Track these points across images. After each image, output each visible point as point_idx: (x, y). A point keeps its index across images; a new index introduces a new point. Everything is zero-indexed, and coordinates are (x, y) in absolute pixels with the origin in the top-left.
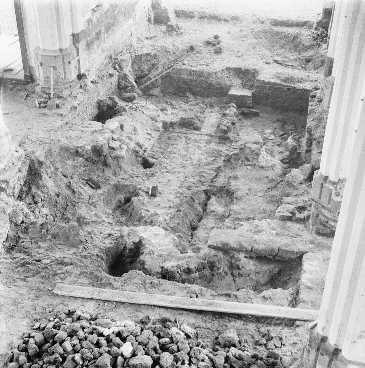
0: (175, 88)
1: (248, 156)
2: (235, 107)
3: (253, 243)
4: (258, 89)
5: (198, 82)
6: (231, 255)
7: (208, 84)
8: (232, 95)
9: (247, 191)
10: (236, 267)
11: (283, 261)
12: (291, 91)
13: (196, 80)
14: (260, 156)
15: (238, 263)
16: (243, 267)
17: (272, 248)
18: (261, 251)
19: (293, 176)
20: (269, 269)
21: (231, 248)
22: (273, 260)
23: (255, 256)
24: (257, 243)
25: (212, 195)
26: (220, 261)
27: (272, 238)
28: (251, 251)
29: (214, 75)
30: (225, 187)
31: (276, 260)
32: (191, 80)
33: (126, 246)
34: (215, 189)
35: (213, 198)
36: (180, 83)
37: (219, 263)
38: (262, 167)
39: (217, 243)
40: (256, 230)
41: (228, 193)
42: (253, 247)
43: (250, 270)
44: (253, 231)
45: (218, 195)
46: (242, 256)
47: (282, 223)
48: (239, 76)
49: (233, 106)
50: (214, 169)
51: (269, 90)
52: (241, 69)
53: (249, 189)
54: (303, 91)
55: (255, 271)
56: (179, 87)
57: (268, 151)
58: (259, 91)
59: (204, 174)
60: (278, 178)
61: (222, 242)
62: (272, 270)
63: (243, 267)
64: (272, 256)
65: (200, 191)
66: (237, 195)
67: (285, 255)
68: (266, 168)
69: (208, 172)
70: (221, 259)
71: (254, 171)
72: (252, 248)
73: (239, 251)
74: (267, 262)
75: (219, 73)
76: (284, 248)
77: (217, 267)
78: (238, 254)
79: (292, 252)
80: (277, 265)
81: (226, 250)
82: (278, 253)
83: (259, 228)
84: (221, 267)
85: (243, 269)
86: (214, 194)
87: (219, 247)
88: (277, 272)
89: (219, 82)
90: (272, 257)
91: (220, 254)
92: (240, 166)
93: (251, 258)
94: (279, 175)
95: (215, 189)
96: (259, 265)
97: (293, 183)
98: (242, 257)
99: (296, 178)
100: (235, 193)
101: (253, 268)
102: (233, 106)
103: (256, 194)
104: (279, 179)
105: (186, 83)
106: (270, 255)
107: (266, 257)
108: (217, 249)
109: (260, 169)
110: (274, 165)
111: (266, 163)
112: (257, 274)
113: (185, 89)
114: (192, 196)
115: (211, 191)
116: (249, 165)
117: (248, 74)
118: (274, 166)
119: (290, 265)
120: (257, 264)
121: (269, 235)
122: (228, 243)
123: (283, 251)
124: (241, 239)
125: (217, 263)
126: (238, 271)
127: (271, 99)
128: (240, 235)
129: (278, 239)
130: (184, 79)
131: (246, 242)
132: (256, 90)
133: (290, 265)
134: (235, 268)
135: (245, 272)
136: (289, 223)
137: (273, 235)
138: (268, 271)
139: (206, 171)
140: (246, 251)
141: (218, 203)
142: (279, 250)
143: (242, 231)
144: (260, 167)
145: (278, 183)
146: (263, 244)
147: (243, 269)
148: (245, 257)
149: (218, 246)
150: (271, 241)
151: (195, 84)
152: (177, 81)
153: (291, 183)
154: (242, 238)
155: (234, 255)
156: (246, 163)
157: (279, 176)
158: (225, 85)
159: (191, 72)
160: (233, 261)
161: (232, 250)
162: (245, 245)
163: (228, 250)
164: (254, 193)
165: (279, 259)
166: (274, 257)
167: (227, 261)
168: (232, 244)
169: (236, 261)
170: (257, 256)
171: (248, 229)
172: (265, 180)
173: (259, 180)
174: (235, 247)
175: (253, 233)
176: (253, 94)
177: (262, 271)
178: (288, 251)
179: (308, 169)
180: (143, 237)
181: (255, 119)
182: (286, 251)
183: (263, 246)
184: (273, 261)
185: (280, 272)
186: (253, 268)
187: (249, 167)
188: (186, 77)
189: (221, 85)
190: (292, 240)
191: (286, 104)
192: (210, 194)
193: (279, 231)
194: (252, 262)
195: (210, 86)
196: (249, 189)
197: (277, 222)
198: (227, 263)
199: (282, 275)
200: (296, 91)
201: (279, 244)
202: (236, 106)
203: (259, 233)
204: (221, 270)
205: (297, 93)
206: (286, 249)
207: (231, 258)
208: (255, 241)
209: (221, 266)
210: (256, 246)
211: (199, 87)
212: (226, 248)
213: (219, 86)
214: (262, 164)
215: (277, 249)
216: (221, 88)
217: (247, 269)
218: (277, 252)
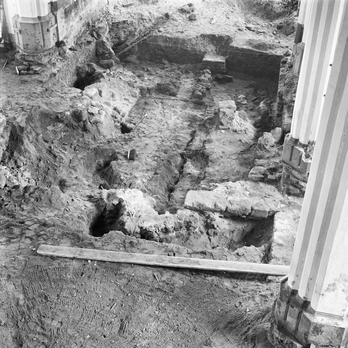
0: (151, 55)
4: (231, 56)
6: (207, 215)
11: (255, 220)
14: (234, 120)
16: (218, 226)
18: (235, 211)
19: (265, 139)
23: (229, 216)
25: (188, 158)
27: (245, 198)
31: (249, 219)
33: (106, 207)
34: (191, 152)
37: (195, 222)
38: (235, 131)
43: (225, 229)
46: (216, 216)
52: (215, 35)
53: (223, 152)
57: (241, 116)
63: (218, 226)
68: (240, 132)
69: (184, 136)
72: (226, 209)
73: (214, 211)
75: (193, 40)
80: (250, 224)
82: (251, 212)
84: (197, 227)
90: (245, 217)
91: (196, 214)
93: (226, 217)
95: (191, 152)
105: (161, 50)
109: (234, 133)
110: (247, 128)
115: (187, 155)
118: (247, 130)
120: (231, 223)
129: (251, 200)
130: (160, 46)
140: (221, 212)
144: (234, 131)
149: (194, 206)
158: (200, 51)
159: (166, 39)
160: (209, 221)
164: (228, 156)
167: (203, 220)
174: (211, 207)
180: (122, 199)
181: (228, 84)
185: (252, 231)
186: (227, 227)
194: (226, 222)
195: (185, 52)
196: (223, 152)
198: (202, 222)
200: (267, 57)
205: (269, 59)
206: (258, 208)
209: (197, 225)
211: (174, 54)
212: (202, 208)
213: (194, 53)
214: (235, 128)
216: (196, 54)
218: (250, 211)
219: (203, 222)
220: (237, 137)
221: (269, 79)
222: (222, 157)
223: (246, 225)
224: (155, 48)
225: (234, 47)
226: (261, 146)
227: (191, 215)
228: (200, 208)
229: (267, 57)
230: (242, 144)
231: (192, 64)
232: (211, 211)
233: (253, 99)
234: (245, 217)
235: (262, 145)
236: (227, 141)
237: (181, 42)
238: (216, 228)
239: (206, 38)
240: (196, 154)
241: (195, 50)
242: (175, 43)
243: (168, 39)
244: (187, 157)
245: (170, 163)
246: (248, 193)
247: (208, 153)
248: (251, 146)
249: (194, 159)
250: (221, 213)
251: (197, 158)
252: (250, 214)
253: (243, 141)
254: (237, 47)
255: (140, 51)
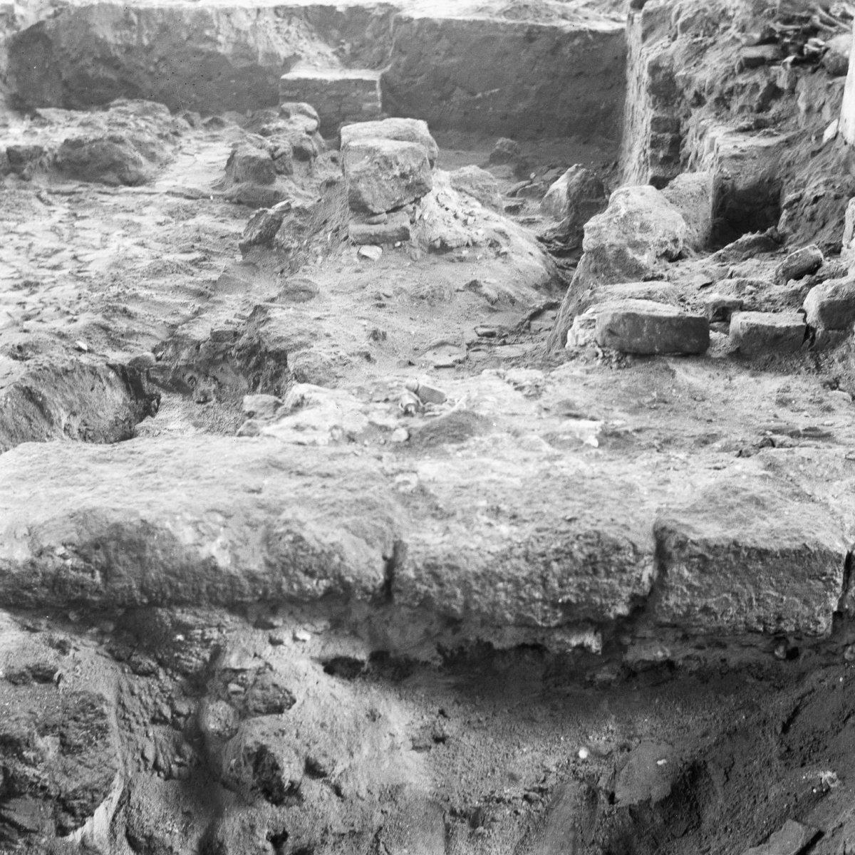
0: (66, 84)
1: (362, 186)
2: (309, 116)
3: (399, 513)
4: (404, 59)
5: (159, 52)
6: (195, 659)
7: (199, 59)
8: (298, 80)
9: (364, 344)
10: (247, 775)
11: (703, 676)
12: (540, 45)
13: (149, 49)
14: (429, 200)
15: (258, 731)
16: (312, 769)
17: (597, 539)
18: (488, 577)
19: (624, 220)
20: (573, 768)
21: (181, 573)
22: (604, 675)
23: (426, 654)
24: (439, 513)
25: (168, 389)
26: (79, 725)
27: (572, 464)
28: (389, 589)
29: (223, 19)
30: (236, 335)
31: (630, 673)
32: (129, 49)
34: (184, 354)
35: (172, 406)
36: (88, 61)
37: (66, 747)
38: (441, 249)
39: (32, 534)
40: (418, 423)
41: (259, 365)
42: (398, 547)
43: (393, 793)
44: (402, 435)
45: (204, 386)
46: (293, 655)
47: (632, 377)
48: (326, 38)
49: (303, 112)
50: (193, 287)
51: (450, 53)
52: (332, 8)
53: (375, 335)
54: (587, 42)
55: (439, 804)
56: (82, 77)
57: (467, 188)
58: (409, 68)
59: (132, 308)
60: (534, 294)
61: (81, 518)
62: (604, 770)
63: (312, 769)
64: (597, 623)
65: (93, 371)
66: (301, 361)
67: (729, 606)
68: (465, 252)
69: (159, 299)
70: (90, 705)
71: (400, 267)
72: (391, 565)
73: (263, 604)
74: (544, 698)
75: (243, 16)
76: (711, 531)
77: (41, 792)
78: (260, 636)
79: (802, 562)
80: (645, 723)
81: (131, 607)
82: (659, 585)
83: (443, 412)
84: (96, 794)
85: (314, 790)
86: (179, 387)
87: (56, 582)
88: (659, 791)
89: (247, 47)
90: (592, 641)
91: (88, 667)
92: (327, 252)
93: (390, 669)
94: (536, 278)
95: (184, 354)
96: (470, 741)
97: (630, 252)
98: (304, 664)
99: (644, 228)
100: (290, 356)
101: (416, 773)
102: (303, 112)
103: (415, 360)
104: (539, 300)
105: (110, 62)
106: (577, 617)
107: (538, 649)
108: (39, 608)
109: (433, 258)
110: (502, 233)
111: (457, 225)
112: (463, 828)
113: (109, 84)
114: (30, 383)
115: (163, 370)
116: (374, 241)
117: (364, 23)
118: (502, 240)
119: (781, 703)
120: (450, 728)
121: (547, 448)
122: (147, 528)
123: (710, 560)
124: (280, 487)
125: (48, 744)
126: (267, 812)
127: (459, 95)
128: (273, 465)
129: (635, 470)
130: (102, 44)
131: (333, 511)
132: (398, 65)
133: (781, 703)
134: (234, 785)
135: (333, 812)
136: (689, 375)
137: (578, 444)
138: (574, 790)
139: (143, 293)
140: (336, 603)
141: (196, 425)
142: (662, 556)
143: (300, 437)
145: (537, 314)
146: (497, 512)
147: (314, 790)
148: (332, 666)
149: (51, 564)
150: (571, 485)
151: (148, 63)
152: (74, 55)
153: (620, 253)
154: (297, 482)
155: (217, 652)
156: (356, 228)
157: (536, 287)
158: (272, 56)
159: (127, 15)
160: (216, 716)
161: (194, 603)
162: (321, 532)
163: (159, 598)
164: (404, 356)
165: (659, 653)
166: (617, 633)
167: (157, 720)
168: (187, 536)
169: (244, 713)
170: (449, 640)
171: (358, 426)
172: (465, 299)
173: (428, 300)
174: (224, 561)
175: (398, 447)
176: (384, 79)
177: (508, 791)
178: (763, 554)
179: (703, 192)
182: (740, 560)
183: (504, 529)
184: (606, 685)
185: (686, 791)
186: (416, 773)
187: (373, 252)
188: (108, 34)
189: (255, 57)
190: (771, 466)
191: (521, 106)
192: (156, 389)
193: (622, 421)
194: (401, 717)
195: (210, 65)
196: (375, 335)
197: (595, 378)
198: (154, 741)
199: (710, 815)
200: (559, 45)
201: (653, 504)
202: (315, 113)
203: (450, 447)
204: (99, 823)
205: (566, 50)
206: (732, 534)
207: (200, 684)
208: (422, 500)
209: (88, 777)
210: (428, 541)
211: (163, 76)
212: (127, 581)
213: (246, 63)
214: (440, 231)
215: (648, 545)
216: (255, 69)
217: (357, 785)
218: (648, 571)
219: (156, 731)
220: (449, 274)
221: (573, 138)
222: (368, 357)
223: (604, 736)
224: (82, 54)
225: (410, 20)
226: (604, 260)
227: (20, 664)
228: (107, 572)
229: (559, 45)
230: (482, 301)
231: (243, 112)
232: (236, 607)
233: (509, 191)
234: (592, 641)
235: (610, 253)
236: (400, 292)
237: (187, 21)
238: (294, 790)
239: (294, 18)
240: (212, 362)
241: (243, 50)
242: (164, 29)
243: (135, 18)
244: (163, 386)
245: (41, 406)
246: (588, 430)
247: (280, 340)
248: (537, 314)
249: (205, 394)
250: (337, 625)
251: (221, 386)
252: (640, 606)
253: (486, 289)
254: (422, 21)
255: (16, 73)
